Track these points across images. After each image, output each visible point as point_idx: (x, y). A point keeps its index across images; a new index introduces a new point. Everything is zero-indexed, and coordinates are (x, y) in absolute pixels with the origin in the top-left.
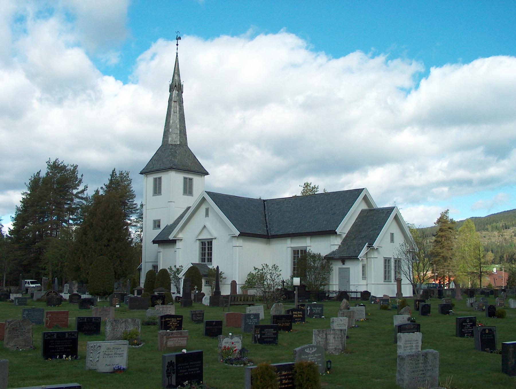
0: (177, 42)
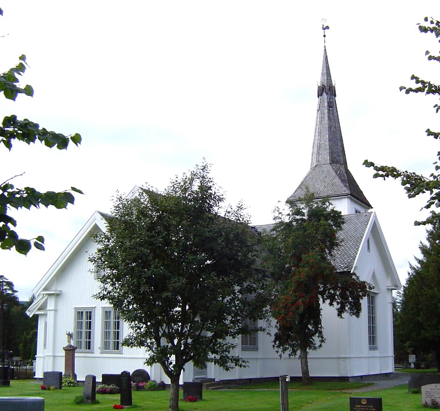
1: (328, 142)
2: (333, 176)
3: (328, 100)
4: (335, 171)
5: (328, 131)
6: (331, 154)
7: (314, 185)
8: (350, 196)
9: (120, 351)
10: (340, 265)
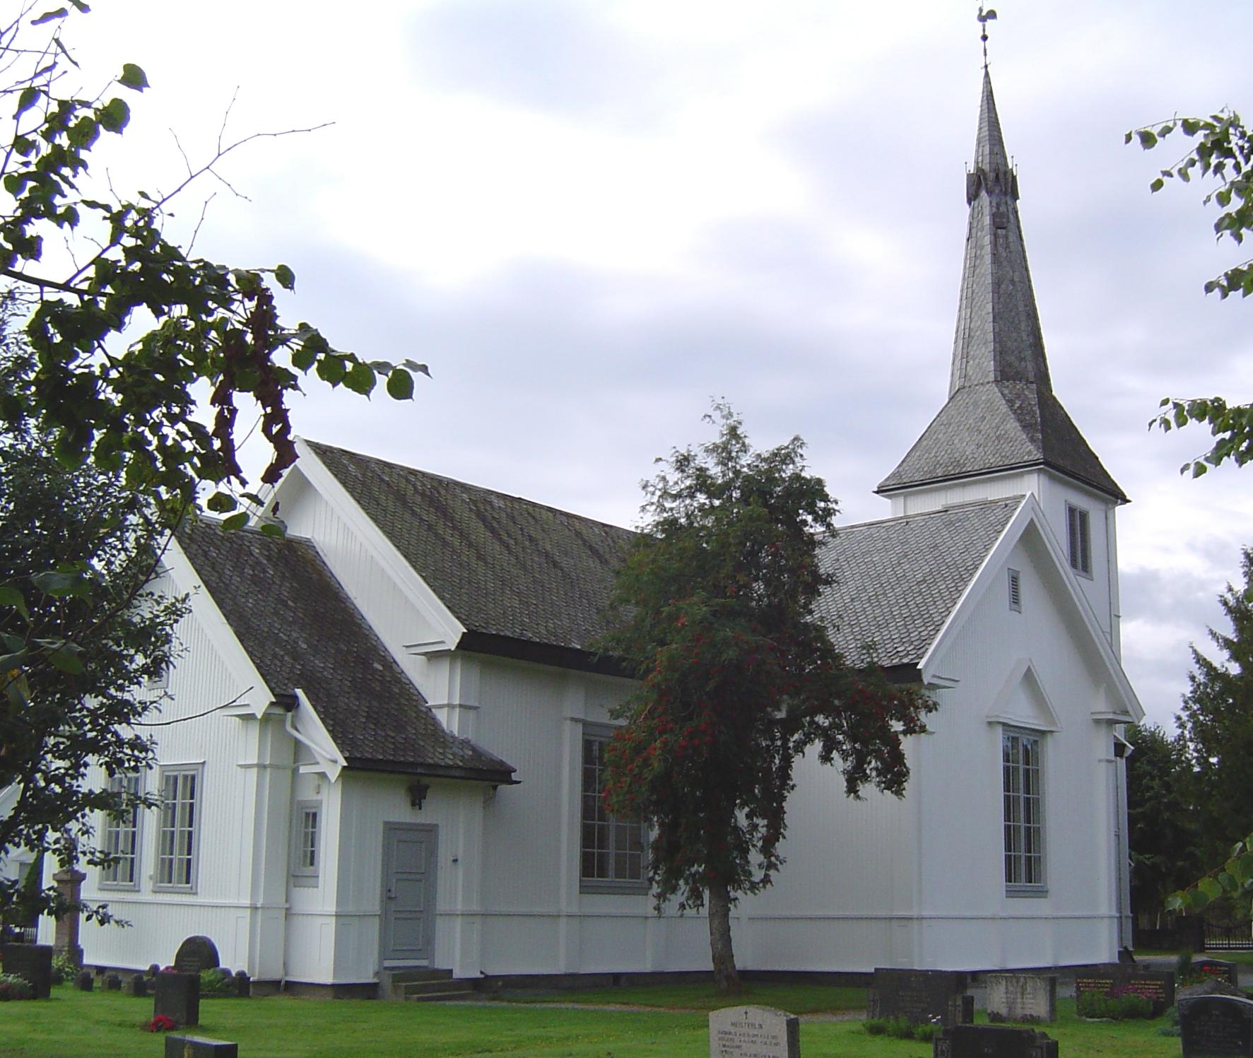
0: (984, 30)
1: (991, 324)
2: (1001, 415)
3: (994, 210)
4: (1008, 401)
5: (993, 292)
6: (1001, 353)
7: (950, 443)
8: (1042, 466)
9: (191, 888)
10: (896, 648)
